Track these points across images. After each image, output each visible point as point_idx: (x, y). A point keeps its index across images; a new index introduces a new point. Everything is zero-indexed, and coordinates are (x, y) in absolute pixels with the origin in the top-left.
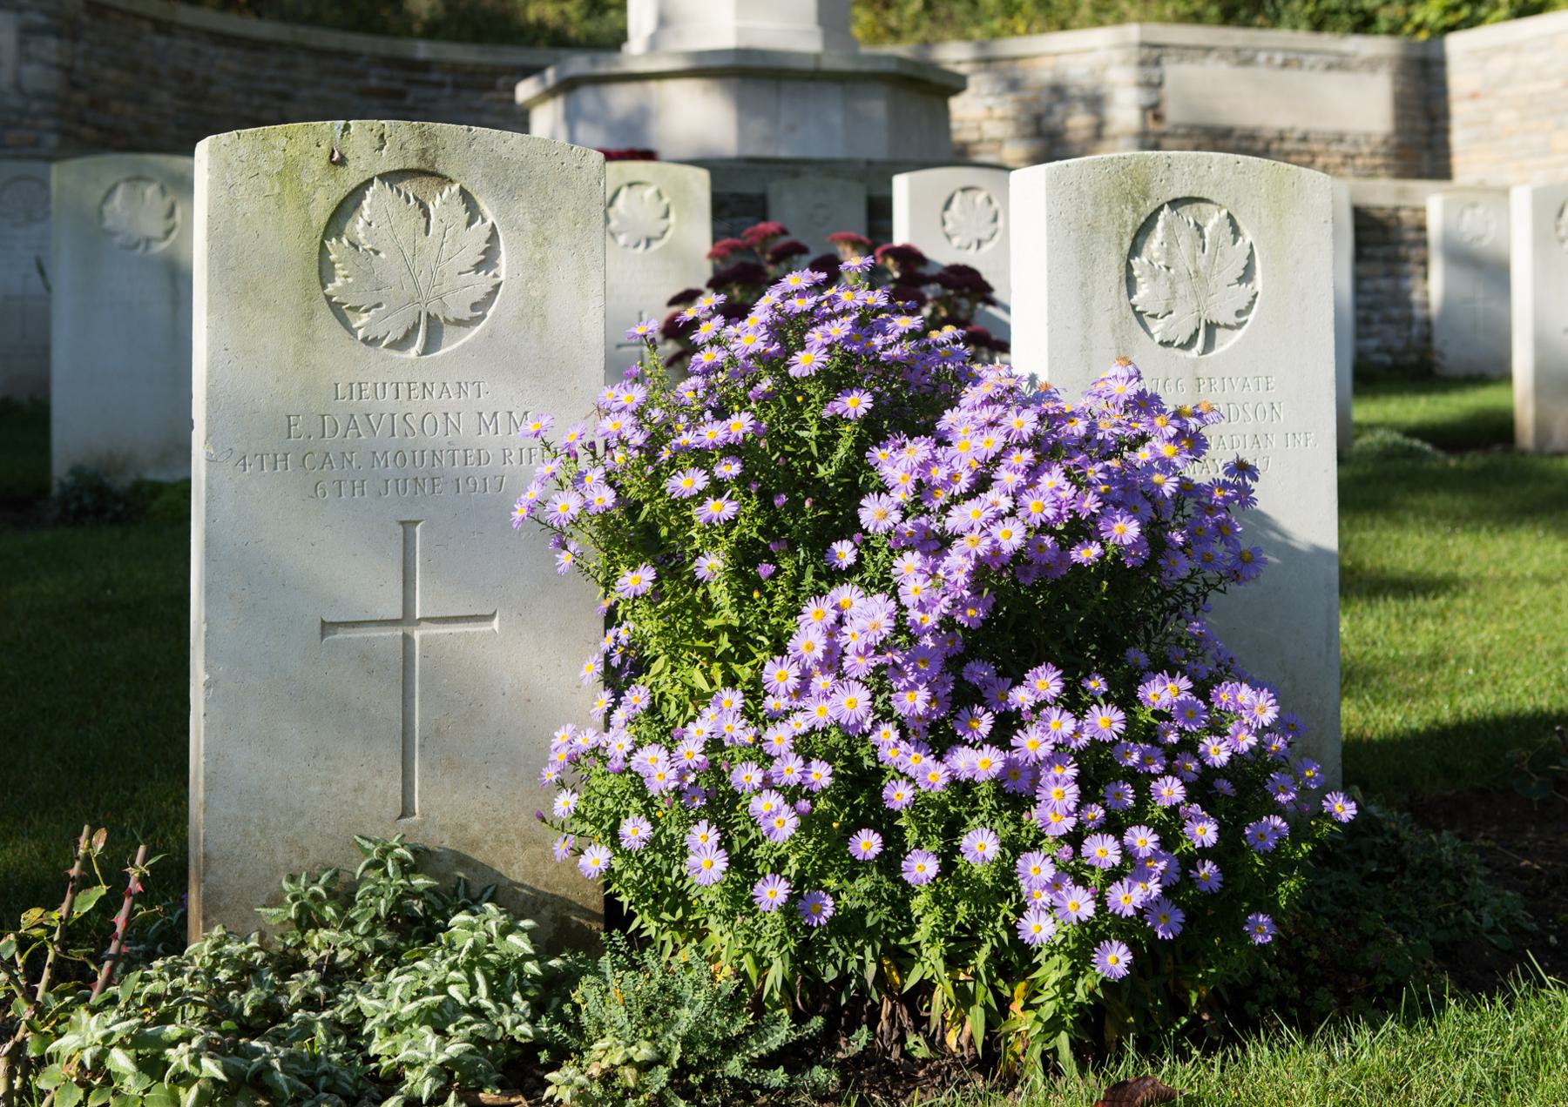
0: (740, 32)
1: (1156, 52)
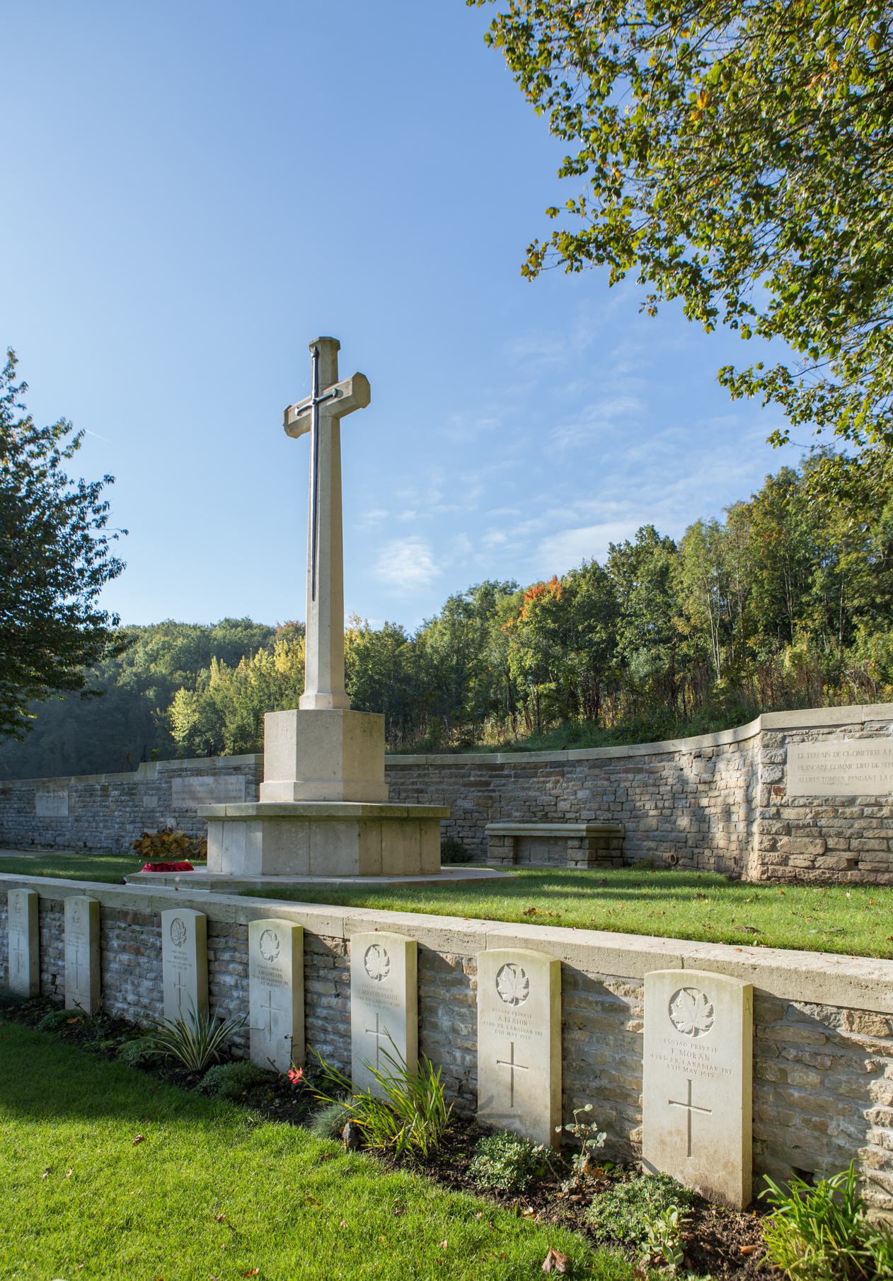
1: (780, 735)
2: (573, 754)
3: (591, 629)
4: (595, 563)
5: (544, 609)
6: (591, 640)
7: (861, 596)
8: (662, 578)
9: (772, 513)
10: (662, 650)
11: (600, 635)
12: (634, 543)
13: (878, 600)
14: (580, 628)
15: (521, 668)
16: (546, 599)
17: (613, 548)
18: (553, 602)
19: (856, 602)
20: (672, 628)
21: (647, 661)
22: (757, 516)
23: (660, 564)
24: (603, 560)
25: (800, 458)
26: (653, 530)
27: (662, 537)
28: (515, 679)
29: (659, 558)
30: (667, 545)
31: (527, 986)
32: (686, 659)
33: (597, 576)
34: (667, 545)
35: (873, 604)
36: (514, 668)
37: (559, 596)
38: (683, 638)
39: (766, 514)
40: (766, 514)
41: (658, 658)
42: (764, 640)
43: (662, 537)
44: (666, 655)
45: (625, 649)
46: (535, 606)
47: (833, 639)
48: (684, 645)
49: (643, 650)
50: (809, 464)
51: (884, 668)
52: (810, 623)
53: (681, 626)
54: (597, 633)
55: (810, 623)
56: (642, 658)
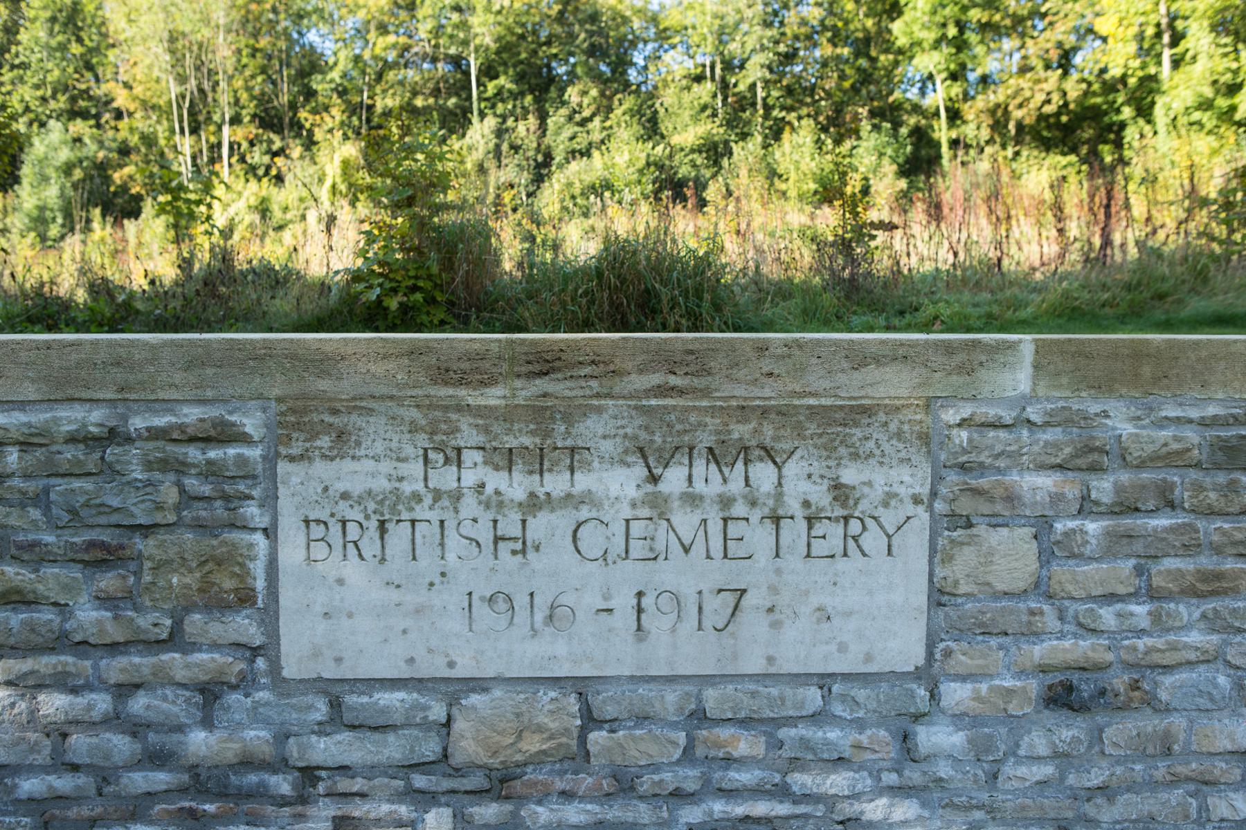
10: (79, 127)
19: (390, 102)
21: (65, 142)
53: (122, 100)
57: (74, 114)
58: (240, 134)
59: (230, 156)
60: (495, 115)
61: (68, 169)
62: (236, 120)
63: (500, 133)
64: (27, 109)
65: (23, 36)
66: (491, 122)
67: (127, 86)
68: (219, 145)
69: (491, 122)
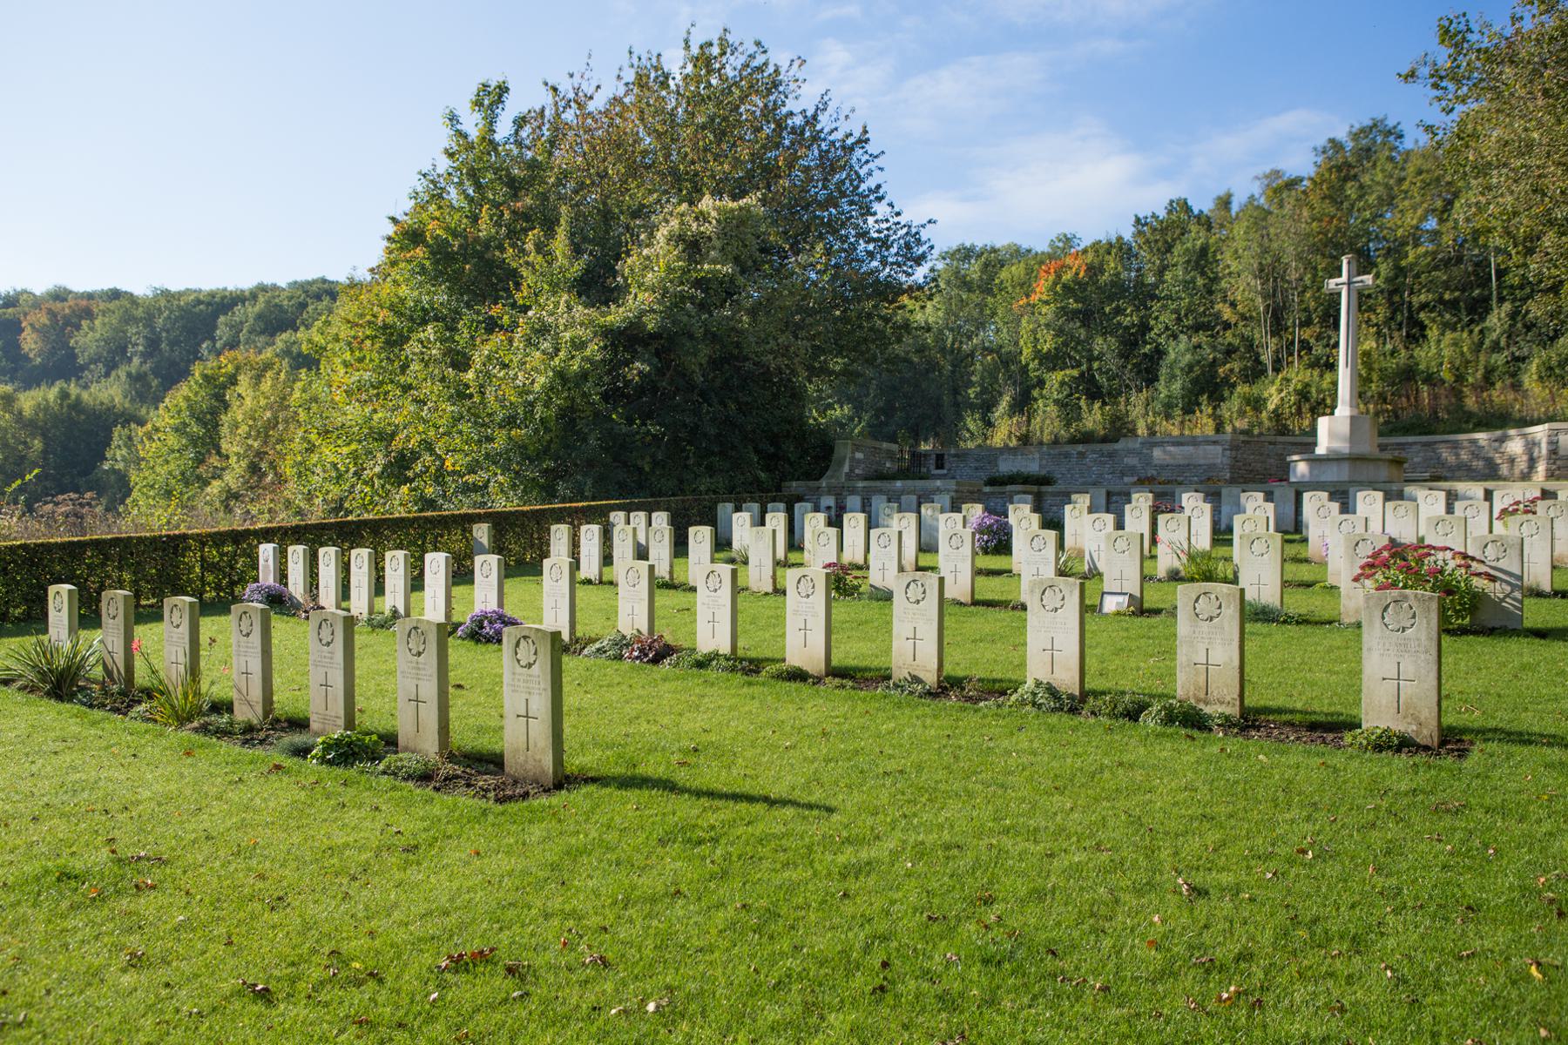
0: (1328, 448)
2: (1410, 439)
3: (1118, 311)
4: (1120, 238)
5: (1065, 286)
6: (1119, 324)
7: (1428, 291)
8: (1202, 259)
9: (1330, 197)
10: (1201, 337)
11: (1130, 319)
12: (1162, 214)
13: (1447, 297)
14: (1107, 310)
15: (1037, 354)
16: (1069, 276)
17: (1138, 220)
18: (1076, 280)
19: (1423, 298)
20: (1218, 315)
21: (1188, 350)
22: (1314, 199)
23: (1199, 243)
24: (1128, 234)
25: (1348, 129)
26: (1186, 203)
27: (1196, 212)
28: (1027, 365)
29: (1196, 237)
30: (1203, 221)
31: (1220, 607)
32: (1230, 351)
33: (1120, 249)
34: (1203, 221)
35: (1441, 301)
36: (1027, 352)
37: (1082, 274)
38: (1227, 326)
39: (1323, 198)
40: (1323, 198)
41: (1199, 346)
42: (1320, 333)
43: (1196, 212)
44: (1207, 343)
45: (1159, 335)
46: (1055, 284)
47: (1396, 334)
48: (1229, 333)
49: (1183, 337)
50: (1355, 136)
51: (1458, 369)
52: (1373, 317)
53: (1227, 314)
54: (1126, 316)
55: (1373, 317)
56: (1182, 346)
57: (1197, 328)
58: (1307, 334)
59: (1299, 352)
60: (1514, 301)
61: (1190, 367)
62: (1307, 323)
63: (1513, 316)
64: (1167, 328)
65: (1168, 276)
66: (1507, 306)
67: (1233, 305)
68: (1293, 343)
69: (1507, 306)
